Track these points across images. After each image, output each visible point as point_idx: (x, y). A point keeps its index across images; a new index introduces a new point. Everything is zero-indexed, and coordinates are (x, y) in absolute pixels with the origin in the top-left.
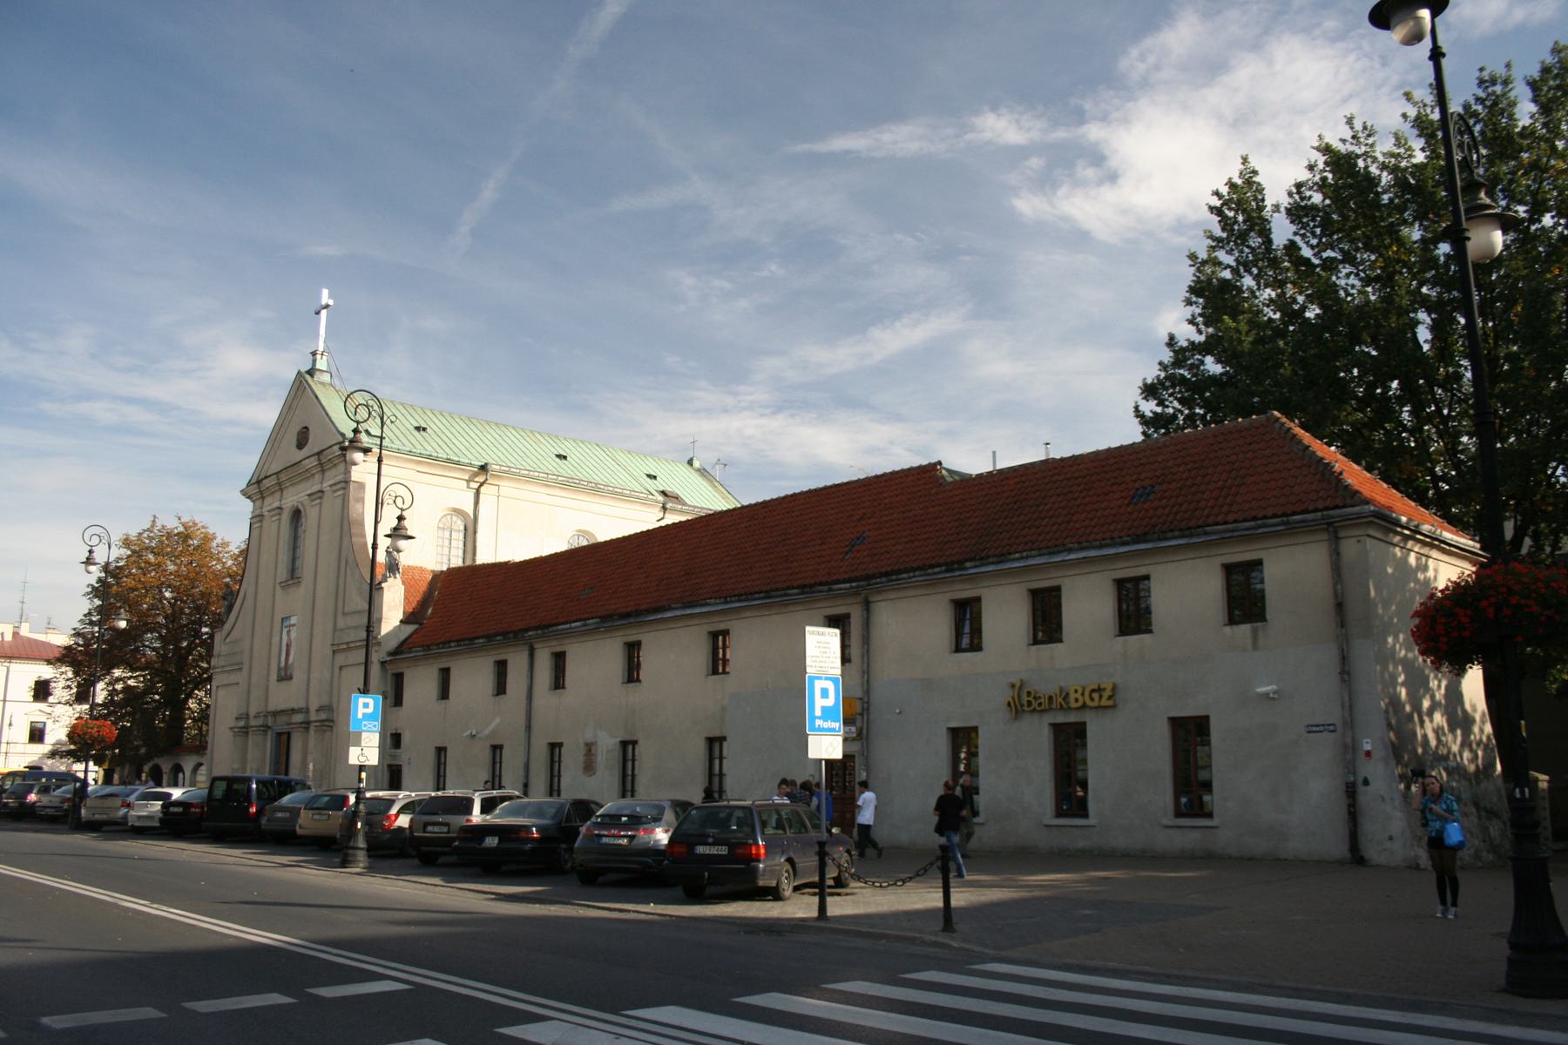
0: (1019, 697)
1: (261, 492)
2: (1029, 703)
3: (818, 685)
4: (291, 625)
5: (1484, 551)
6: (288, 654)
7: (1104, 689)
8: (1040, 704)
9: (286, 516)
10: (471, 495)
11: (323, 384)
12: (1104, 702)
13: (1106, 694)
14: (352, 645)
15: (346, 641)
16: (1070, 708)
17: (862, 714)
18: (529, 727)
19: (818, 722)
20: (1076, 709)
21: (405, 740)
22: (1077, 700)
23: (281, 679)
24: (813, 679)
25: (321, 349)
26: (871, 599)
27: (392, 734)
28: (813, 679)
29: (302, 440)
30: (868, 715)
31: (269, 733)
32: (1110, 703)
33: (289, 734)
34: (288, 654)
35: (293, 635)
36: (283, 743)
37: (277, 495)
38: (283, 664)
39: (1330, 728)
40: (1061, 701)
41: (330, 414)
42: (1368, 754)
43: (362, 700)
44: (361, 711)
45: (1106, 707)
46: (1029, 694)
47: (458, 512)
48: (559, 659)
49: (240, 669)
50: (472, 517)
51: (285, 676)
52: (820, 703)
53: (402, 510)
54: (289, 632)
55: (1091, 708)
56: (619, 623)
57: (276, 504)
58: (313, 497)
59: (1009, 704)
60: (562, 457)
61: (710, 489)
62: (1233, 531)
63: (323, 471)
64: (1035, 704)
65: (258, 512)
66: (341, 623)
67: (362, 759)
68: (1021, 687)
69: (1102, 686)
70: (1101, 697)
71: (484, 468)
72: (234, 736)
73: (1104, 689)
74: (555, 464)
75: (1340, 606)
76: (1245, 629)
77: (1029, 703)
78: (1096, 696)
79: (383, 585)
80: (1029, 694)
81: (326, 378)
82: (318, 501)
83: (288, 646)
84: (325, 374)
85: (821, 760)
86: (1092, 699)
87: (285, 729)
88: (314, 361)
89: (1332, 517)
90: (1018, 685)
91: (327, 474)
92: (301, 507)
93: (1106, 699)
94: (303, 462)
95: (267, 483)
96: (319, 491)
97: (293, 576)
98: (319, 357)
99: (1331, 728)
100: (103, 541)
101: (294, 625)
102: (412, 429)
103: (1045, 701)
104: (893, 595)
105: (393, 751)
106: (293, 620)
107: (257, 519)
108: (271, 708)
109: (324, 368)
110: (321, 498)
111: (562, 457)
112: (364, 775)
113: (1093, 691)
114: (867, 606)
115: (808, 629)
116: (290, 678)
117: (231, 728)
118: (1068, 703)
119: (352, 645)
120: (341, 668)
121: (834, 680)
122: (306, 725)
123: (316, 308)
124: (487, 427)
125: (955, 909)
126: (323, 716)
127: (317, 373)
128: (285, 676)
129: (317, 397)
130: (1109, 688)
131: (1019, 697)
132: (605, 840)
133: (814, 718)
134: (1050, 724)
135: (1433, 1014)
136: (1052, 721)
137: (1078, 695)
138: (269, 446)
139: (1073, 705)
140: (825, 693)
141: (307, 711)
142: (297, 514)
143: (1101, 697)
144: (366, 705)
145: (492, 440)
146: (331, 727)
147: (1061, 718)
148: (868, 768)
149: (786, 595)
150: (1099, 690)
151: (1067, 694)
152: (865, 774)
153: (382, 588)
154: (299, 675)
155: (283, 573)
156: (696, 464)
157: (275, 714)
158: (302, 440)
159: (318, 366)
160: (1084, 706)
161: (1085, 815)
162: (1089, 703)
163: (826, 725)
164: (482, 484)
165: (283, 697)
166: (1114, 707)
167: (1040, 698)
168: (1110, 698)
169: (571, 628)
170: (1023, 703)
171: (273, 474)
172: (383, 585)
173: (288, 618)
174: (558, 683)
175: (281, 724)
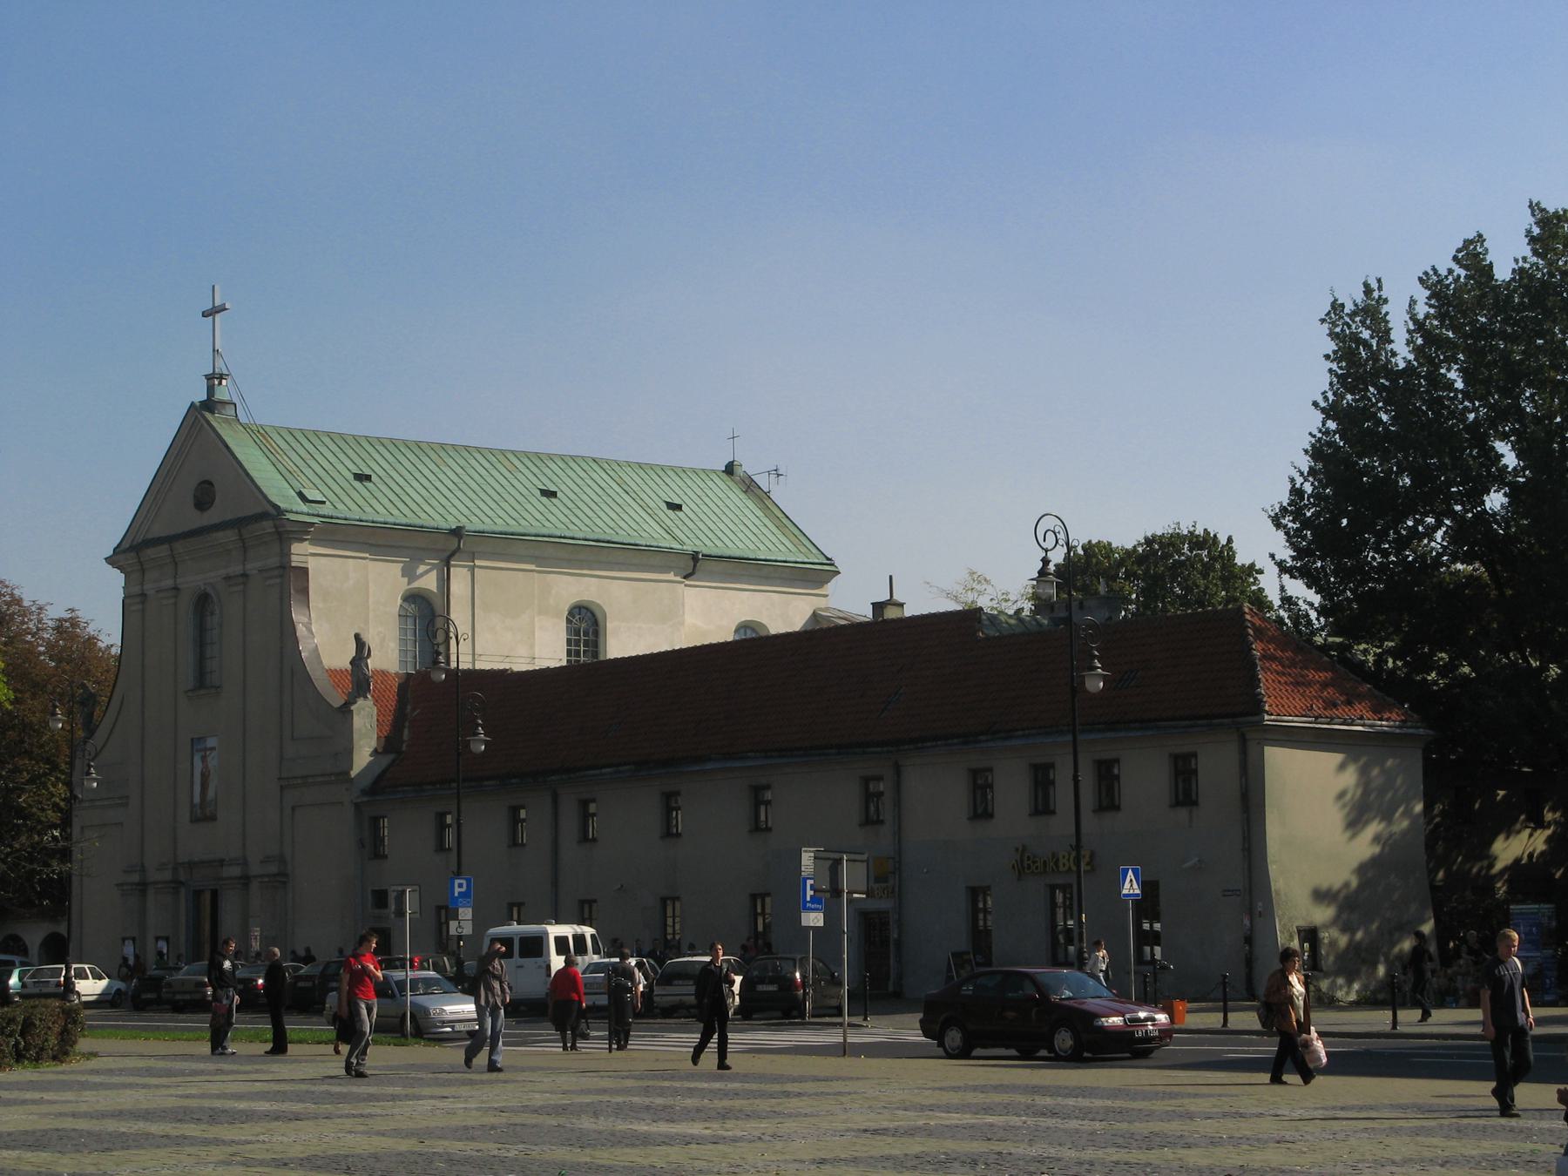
0: (1022, 861)
4: (206, 749)
14: (310, 780)
17: (894, 873)
18: (555, 883)
19: (808, 905)
22: (1064, 865)
23: (195, 820)
27: (374, 892)
29: (204, 497)
31: (183, 891)
33: (215, 895)
35: (213, 762)
38: (197, 799)
43: (457, 882)
44: (457, 890)
48: (584, 804)
51: (204, 815)
59: (1013, 867)
61: (759, 513)
65: (136, 590)
74: (542, 509)
76: (1183, 813)
77: (1029, 867)
79: (352, 708)
84: (227, 406)
90: (1020, 849)
92: (209, 590)
97: (202, 681)
99: (1238, 893)
100: (1061, 542)
101: (213, 749)
102: (664, 507)
105: (377, 911)
106: (211, 742)
107: (134, 604)
109: (226, 398)
116: (213, 818)
117: (117, 885)
118: (1057, 867)
124: (443, 454)
125: (471, 1003)
127: (219, 406)
128: (204, 815)
129: (227, 447)
133: (805, 902)
137: (1065, 861)
141: (244, 862)
144: (460, 886)
146: (285, 883)
156: (738, 471)
157: (191, 865)
158: (204, 497)
172: (352, 708)
173: (201, 739)
174: (584, 838)
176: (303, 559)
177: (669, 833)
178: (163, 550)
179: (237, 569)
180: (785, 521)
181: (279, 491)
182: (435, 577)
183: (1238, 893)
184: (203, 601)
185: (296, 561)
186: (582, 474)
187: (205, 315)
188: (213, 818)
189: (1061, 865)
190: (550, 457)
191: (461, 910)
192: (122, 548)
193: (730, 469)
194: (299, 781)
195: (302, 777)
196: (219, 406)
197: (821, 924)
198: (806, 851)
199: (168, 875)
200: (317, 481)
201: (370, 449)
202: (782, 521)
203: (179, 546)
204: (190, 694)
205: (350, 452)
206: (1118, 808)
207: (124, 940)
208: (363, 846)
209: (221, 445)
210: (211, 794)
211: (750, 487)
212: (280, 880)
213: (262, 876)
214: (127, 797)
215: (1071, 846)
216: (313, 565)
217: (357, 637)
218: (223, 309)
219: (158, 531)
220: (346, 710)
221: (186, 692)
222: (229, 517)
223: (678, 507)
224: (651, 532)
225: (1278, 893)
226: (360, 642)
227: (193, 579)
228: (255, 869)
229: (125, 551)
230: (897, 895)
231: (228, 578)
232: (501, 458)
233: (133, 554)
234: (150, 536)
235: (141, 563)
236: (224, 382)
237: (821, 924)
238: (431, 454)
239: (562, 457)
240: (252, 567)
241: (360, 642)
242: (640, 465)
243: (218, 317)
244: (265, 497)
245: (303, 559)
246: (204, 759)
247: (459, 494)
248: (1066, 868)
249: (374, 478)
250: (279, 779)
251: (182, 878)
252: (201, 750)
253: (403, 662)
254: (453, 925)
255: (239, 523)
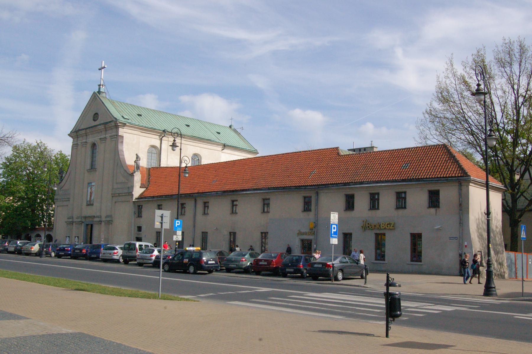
0: (365, 225)
1: (77, 136)
2: (369, 227)
3: (333, 226)
4: (92, 186)
5: (505, 187)
6: (91, 196)
7: (391, 224)
8: (372, 227)
9: (89, 146)
10: (159, 142)
11: (103, 97)
12: (391, 228)
13: (392, 225)
14: (121, 195)
15: (118, 193)
16: (381, 229)
18: (194, 226)
19: (333, 235)
20: (383, 229)
21: (143, 229)
22: (383, 226)
23: (88, 205)
24: (332, 225)
25: (102, 84)
26: (319, 192)
28: (332, 225)
29: (96, 116)
30: (317, 227)
32: (393, 228)
33: (92, 225)
34: (91, 196)
35: (93, 189)
36: (90, 228)
37: (85, 137)
38: (89, 199)
39: (456, 238)
40: (378, 226)
41: (109, 110)
42: (466, 246)
43: (177, 221)
44: (177, 224)
45: (391, 229)
46: (368, 224)
47: (153, 147)
49: (69, 200)
50: (159, 148)
51: (90, 204)
52: (333, 230)
53: (187, 164)
54: (91, 188)
55: (387, 229)
56: (230, 194)
57: (85, 141)
58: (102, 140)
59: (362, 227)
60: (188, 126)
61: (238, 137)
62: (432, 181)
63: (106, 131)
64: (370, 227)
65: (76, 143)
66: (116, 186)
67: (177, 239)
68: (366, 222)
69: (391, 223)
70: (390, 226)
71: (164, 131)
72: (67, 225)
73: (391, 224)
75: (460, 205)
76: (433, 210)
77: (369, 227)
78: (389, 226)
79: (134, 174)
80: (368, 224)
81: (104, 95)
82: (104, 141)
83: (91, 193)
84: (104, 93)
85: (333, 244)
86: (388, 227)
87: (91, 223)
88: (100, 89)
89: (460, 179)
90: (365, 221)
91: (107, 132)
92: (96, 142)
93: (392, 226)
94: (98, 127)
95: (80, 132)
96: (105, 138)
97: (93, 168)
98: (101, 87)
99: (456, 238)
101: (94, 186)
103: (373, 227)
104: (326, 191)
105: (138, 232)
106: (93, 184)
107: (75, 146)
108: (83, 215)
109: (103, 91)
110: (105, 140)
111: (188, 126)
112: (177, 243)
113: (388, 224)
114: (317, 193)
115: (331, 212)
116: (92, 205)
117: (66, 222)
118: (380, 227)
119: (121, 195)
120: (115, 202)
121: (336, 225)
122: (100, 222)
123: (100, 67)
124: (160, 113)
126: (108, 219)
127: (101, 93)
128: (90, 204)
129: (103, 103)
130: (393, 223)
131: (365, 225)
132: (230, 265)
133: (331, 234)
134: (375, 233)
135: (490, 337)
136: (376, 232)
137: (383, 225)
138: (81, 118)
139: (382, 228)
140: (334, 228)
141: (101, 217)
142: (94, 145)
143: (390, 226)
144: (178, 223)
145: (163, 119)
146: (112, 223)
147: (378, 232)
148: (316, 243)
149: (290, 189)
150: (390, 224)
151: (380, 225)
152: (315, 246)
153: (134, 175)
154: (96, 204)
155: (89, 167)
156: (233, 127)
157: (86, 217)
158: (96, 116)
159: (101, 90)
160: (385, 228)
161: (384, 260)
162: (386, 227)
163: (334, 236)
164: (163, 137)
165: (88, 212)
166: (394, 229)
167: (372, 225)
168: (393, 226)
169: (206, 195)
170: (366, 226)
171: (83, 129)
172: (134, 174)
173: (91, 183)
174: (205, 214)
175: (88, 221)
176: (122, 133)
177: (233, 212)
178: (84, 132)
179: (103, 136)
180: (245, 140)
181: (116, 114)
182: (157, 146)
183: (456, 238)
184: (94, 145)
185: (120, 134)
186: (195, 123)
187: (99, 70)
188: (92, 205)
189: (382, 227)
190: (187, 118)
191: (177, 232)
192: (73, 131)
193: (230, 127)
194: (117, 195)
195: (119, 194)
196: (101, 93)
197: (337, 243)
198: (332, 214)
199: (79, 220)
200: (127, 114)
201: (141, 109)
202: (244, 139)
203: (88, 131)
204: (88, 171)
205: (136, 110)
206: (379, 209)
207: (75, 237)
208: (135, 214)
209: (101, 103)
210: (92, 198)
211: (235, 131)
212: (109, 222)
213: (106, 221)
214: (69, 198)
215: (485, 213)
216: (125, 135)
217: (137, 155)
218: (104, 67)
219: (82, 127)
220: (132, 175)
221: (87, 170)
222: (102, 122)
223: (219, 133)
224: (213, 138)
225: (472, 238)
226: (137, 157)
227: (91, 139)
228: (103, 219)
229: (73, 132)
230: (316, 234)
231: (100, 139)
232: (175, 116)
233: (75, 133)
234: (80, 129)
235: (77, 136)
236: (103, 87)
237: (337, 243)
238: (157, 113)
239: (190, 119)
240: (108, 136)
241: (137, 157)
242: (209, 123)
243: (103, 70)
244: (113, 116)
245: (122, 133)
246: (91, 188)
247: (165, 123)
248: (384, 227)
249: (142, 116)
250: (112, 194)
251: (83, 221)
252: (90, 186)
253: (148, 165)
254: (175, 237)
255: (105, 124)
